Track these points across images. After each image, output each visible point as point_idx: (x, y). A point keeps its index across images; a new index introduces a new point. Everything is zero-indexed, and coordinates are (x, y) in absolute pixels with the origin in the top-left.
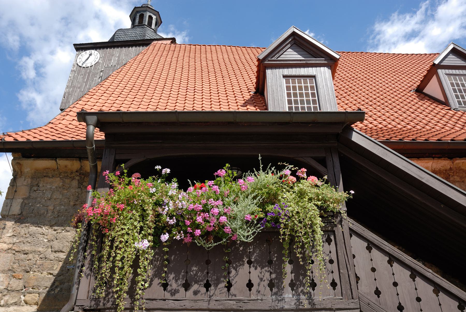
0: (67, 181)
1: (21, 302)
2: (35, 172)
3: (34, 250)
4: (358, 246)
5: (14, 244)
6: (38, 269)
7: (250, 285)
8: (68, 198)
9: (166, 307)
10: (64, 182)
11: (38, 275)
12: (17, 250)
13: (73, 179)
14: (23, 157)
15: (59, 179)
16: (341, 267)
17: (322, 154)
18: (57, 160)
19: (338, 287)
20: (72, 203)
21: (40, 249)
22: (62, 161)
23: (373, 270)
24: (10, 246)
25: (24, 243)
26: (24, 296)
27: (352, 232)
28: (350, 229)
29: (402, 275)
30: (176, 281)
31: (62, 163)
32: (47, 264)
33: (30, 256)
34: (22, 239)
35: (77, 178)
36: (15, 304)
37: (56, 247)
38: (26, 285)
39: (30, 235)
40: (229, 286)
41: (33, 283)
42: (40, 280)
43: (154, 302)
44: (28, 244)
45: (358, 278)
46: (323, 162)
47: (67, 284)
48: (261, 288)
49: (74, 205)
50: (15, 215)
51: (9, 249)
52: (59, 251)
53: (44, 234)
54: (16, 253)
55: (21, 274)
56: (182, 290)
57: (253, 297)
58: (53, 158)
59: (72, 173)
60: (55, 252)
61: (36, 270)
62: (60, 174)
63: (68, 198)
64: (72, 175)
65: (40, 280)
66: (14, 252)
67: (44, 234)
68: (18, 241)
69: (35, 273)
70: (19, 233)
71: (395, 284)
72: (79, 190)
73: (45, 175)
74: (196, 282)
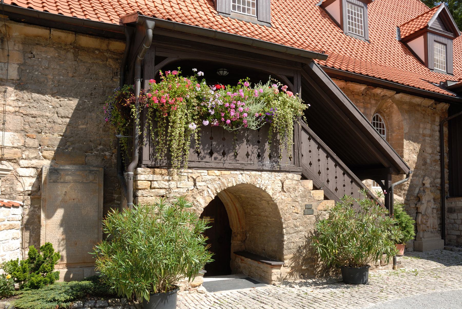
0: (63, 52)
1: (40, 157)
2: (25, 38)
3: (41, 114)
4: (305, 136)
5: (20, 107)
6: (49, 131)
7: (248, 155)
8: (66, 70)
9: (201, 166)
10: (59, 53)
11: (50, 136)
12: (25, 113)
13: (68, 51)
14: (11, 20)
15: (53, 49)
16: (295, 148)
17: (291, 75)
18: (52, 30)
19: (292, 160)
20: (70, 75)
21: (48, 114)
22: (57, 32)
23: (310, 151)
24: (17, 109)
25: (30, 107)
26: (41, 152)
27: (303, 128)
28: (302, 127)
29: (323, 155)
30: (204, 151)
31: (56, 33)
32: (56, 127)
33: (39, 120)
34: (27, 104)
35: (72, 50)
36: (36, 158)
37: (62, 113)
38: (42, 144)
39: (34, 101)
40: (236, 155)
41: (47, 142)
42: (53, 140)
43: (193, 163)
44: (34, 109)
45: (302, 156)
46: (291, 79)
47: (78, 144)
48: (252, 158)
49: (73, 77)
50: (13, 80)
51: (16, 112)
52: (65, 117)
53: (47, 101)
54: (24, 116)
55: (35, 135)
56: (208, 156)
57: (249, 162)
58: (47, 27)
59: (66, 45)
60: (62, 117)
61: (47, 132)
62: (53, 44)
63: (66, 70)
64: (66, 47)
65: (53, 140)
66: (22, 115)
67: (47, 101)
68: (23, 105)
69: (47, 135)
70: (23, 98)
71: (319, 160)
72: (76, 63)
73: (37, 42)
74: (217, 152)
